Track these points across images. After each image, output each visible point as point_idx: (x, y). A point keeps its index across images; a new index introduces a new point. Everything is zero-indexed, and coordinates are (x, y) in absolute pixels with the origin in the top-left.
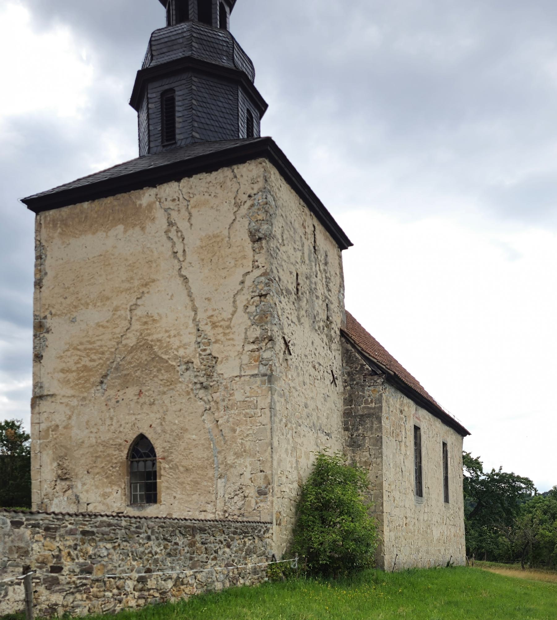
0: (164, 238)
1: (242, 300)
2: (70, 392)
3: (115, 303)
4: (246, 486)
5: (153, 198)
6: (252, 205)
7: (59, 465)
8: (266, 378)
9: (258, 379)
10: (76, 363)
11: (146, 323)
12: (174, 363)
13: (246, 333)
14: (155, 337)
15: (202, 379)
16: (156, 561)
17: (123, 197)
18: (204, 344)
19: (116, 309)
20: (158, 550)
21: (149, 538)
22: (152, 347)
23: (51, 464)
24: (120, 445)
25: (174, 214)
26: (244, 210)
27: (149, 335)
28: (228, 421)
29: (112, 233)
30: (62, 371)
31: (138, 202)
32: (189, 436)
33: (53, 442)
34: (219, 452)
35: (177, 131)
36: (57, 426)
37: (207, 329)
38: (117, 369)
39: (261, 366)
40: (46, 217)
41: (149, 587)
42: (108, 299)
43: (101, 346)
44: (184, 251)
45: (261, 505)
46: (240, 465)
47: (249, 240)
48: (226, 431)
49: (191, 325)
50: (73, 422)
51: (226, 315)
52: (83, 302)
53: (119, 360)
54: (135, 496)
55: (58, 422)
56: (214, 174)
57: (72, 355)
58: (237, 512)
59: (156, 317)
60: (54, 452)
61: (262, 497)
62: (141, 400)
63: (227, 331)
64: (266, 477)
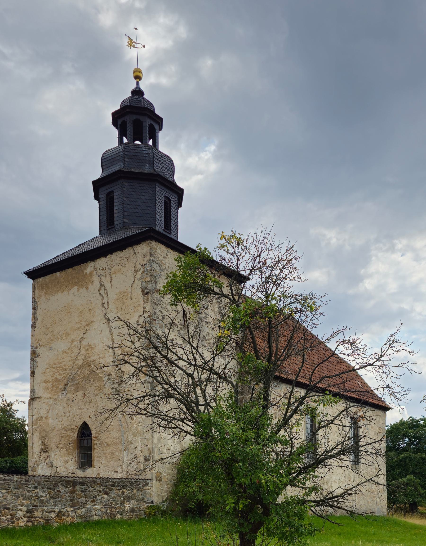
0: (98, 294)
2: (48, 395)
4: (139, 455)
5: (92, 269)
6: (144, 272)
7: (43, 442)
8: (149, 384)
10: (52, 376)
11: (88, 350)
12: (102, 376)
14: (92, 358)
15: (116, 386)
16: (42, 501)
17: (77, 268)
19: (73, 341)
20: (44, 495)
21: (36, 488)
24: (74, 429)
25: (103, 278)
26: (139, 275)
27: (89, 357)
29: (72, 291)
30: (45, 382)
31: (85, 271)
34: (125, 433)
35: (115, 219)
36: (42, 417)
38: (72, 380)
40: (38, 283)
41: (36, 515)
42: (69, 334)
43: (65, 365)
44: (108, 302)
47: (141, 294)
50: (50, 415)
52: (56, 337)
53: (74, 374)
54: (82, 462)
56: (124, 251)
58: (133, 473)
62: (85, 400)
64: (149, 449)
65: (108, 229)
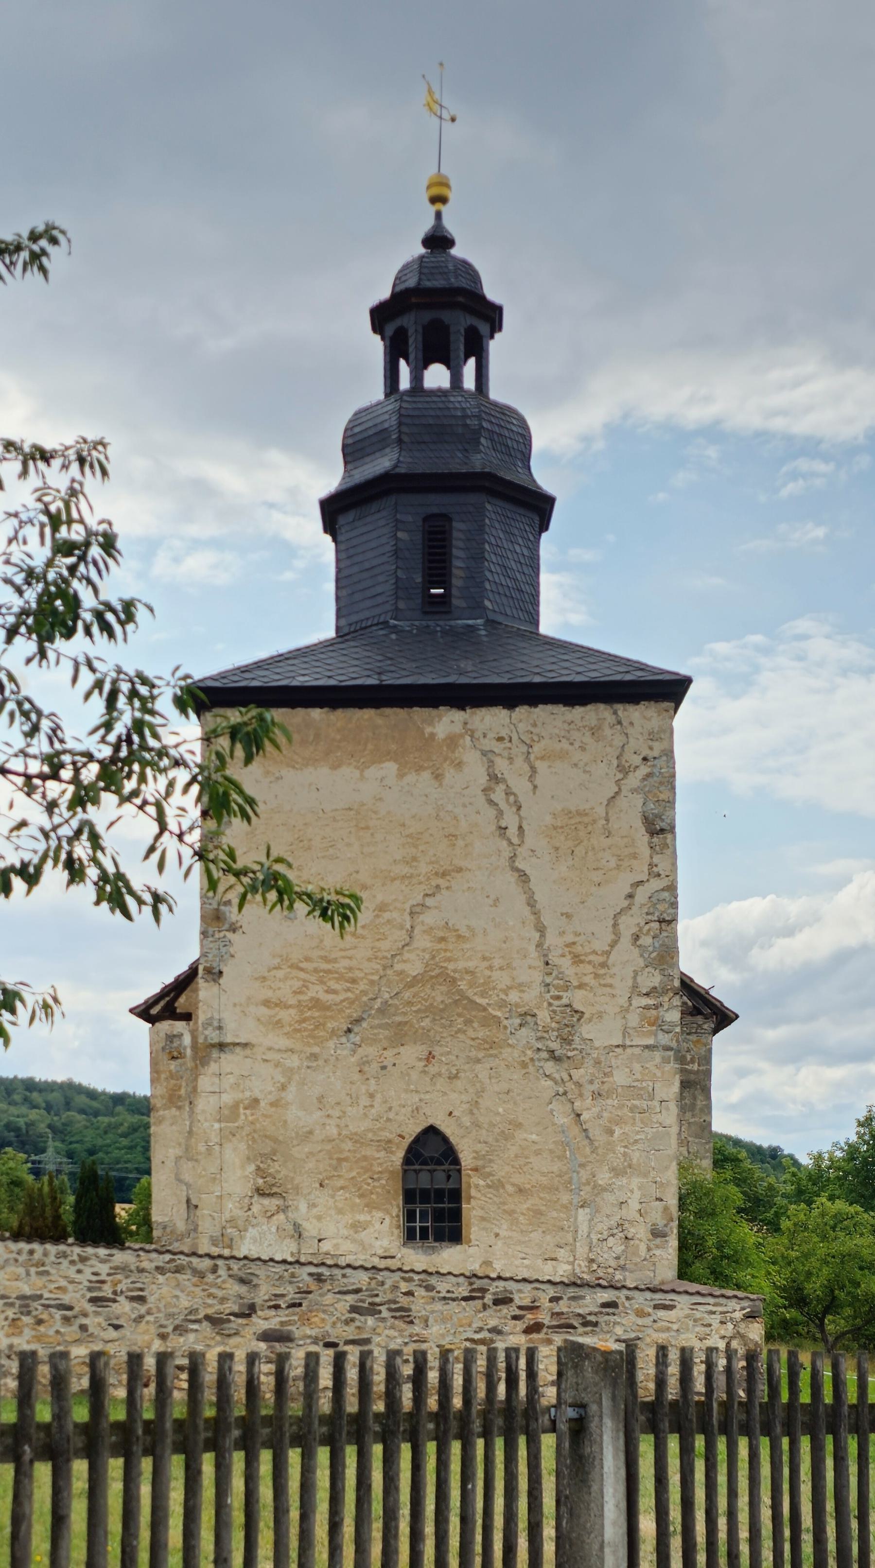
0: (482, 799)
1: (629, 924)
3: (380, 898)
5: (458, 728)
6: (649, 775)
7: (258, 1169)
8: (671, 1053)
9: (658, 1055)
10: (295, 993)
11: (443, 939)
13: (635, 978)
14: (461, 965)
18: (557, 987)
22: (454, 981)
23: (243, 1167)
24: (389, 1141)
26: (634, 780)
28: (600, 1117)
29: (373, 772)
30: (267, 1003)
32: (525, 1135)
33: (247, 1129)
36: (256, 1101)
37: (565, 963)
38: (381, 1011)
39: (660, 1033)
43: (350, 969)
44: (520, 827)
45: (658, 1252)
46: (621, 1188)
48: (596, 1133)
49: (533, 953)
50: (291, 1094)
51: (601, 945)
55: (257, 1094)
56: (579, 711)
57: (286, 978)
58: (613, 1263)
59: (463, 931)
60: (249, 1147)
61: (658, 1241)
62: (433, 1069)
63: (602, 971)
65: (425, 613)
